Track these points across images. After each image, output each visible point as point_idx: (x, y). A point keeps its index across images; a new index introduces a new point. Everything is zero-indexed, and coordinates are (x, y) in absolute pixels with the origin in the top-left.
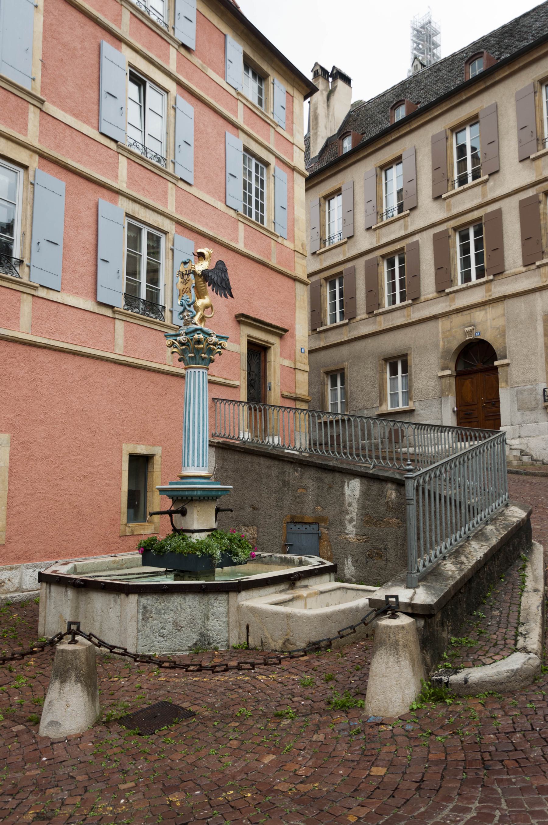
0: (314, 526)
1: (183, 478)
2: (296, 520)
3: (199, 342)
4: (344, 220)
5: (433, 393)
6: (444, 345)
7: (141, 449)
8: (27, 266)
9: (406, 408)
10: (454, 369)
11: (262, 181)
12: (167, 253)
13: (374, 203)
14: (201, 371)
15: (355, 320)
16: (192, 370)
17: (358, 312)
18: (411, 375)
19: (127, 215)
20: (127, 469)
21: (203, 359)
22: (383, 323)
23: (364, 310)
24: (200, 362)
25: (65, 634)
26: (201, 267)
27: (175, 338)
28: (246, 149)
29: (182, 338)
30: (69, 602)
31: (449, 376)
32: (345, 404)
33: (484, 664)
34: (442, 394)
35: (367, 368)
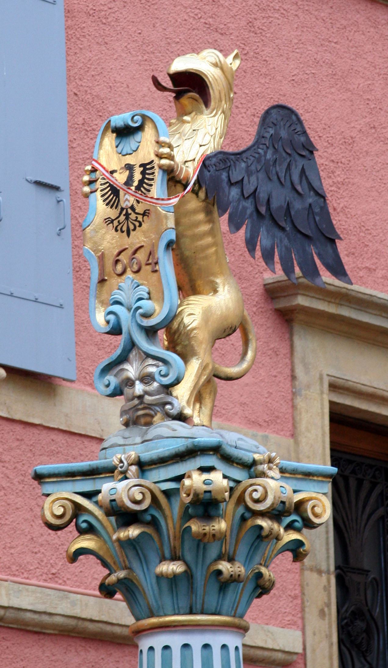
3: (206, 506)
16: (175, 641)
21: (225, 584)
24: (212, 600)
26: (196, 139)
27: (88, 486)
29: (121, 490)
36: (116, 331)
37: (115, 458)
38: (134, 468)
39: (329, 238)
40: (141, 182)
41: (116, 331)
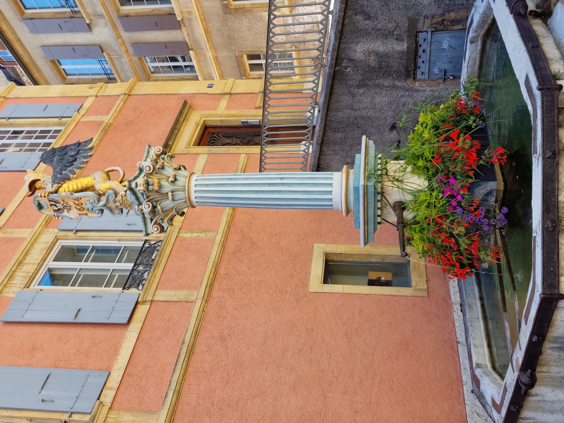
1: (348, 211)
4: (84, 56)
8: (70, 416)
11: (15, 132)
12: (81, 238)
13: (61, 21)
17: (180, 39)
19: (27, 286)
27: (148, 221)
38: (140, 207)
39: (79, 144)
40: (54, 202)
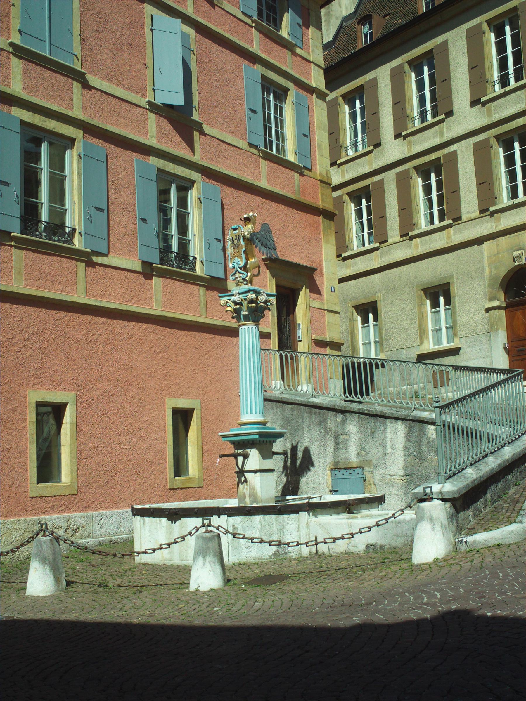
0: (360, 471)
2: (340, 466)
5: (481, 327)
6: (491, 272)
7: (183, 404)
9: (451, 346)
10: (503, 300)
14: (250, 327)
15: (386, 244)
16: (246, 327)
17: (390, 233)
18: (454, 307)
20: (171, 424)
22: (421, 246)
23: (398, 232)
25: (201, 527)
27: (229, 298)
28: (264, 78)
30: (164, 529)
31: (498, 308)
32: (379, 343)
33: (491, 530)
34: (492, 327)
35: (404, 300)
36: (234, 268)
37: (234, 293)
41: (234, 268)
